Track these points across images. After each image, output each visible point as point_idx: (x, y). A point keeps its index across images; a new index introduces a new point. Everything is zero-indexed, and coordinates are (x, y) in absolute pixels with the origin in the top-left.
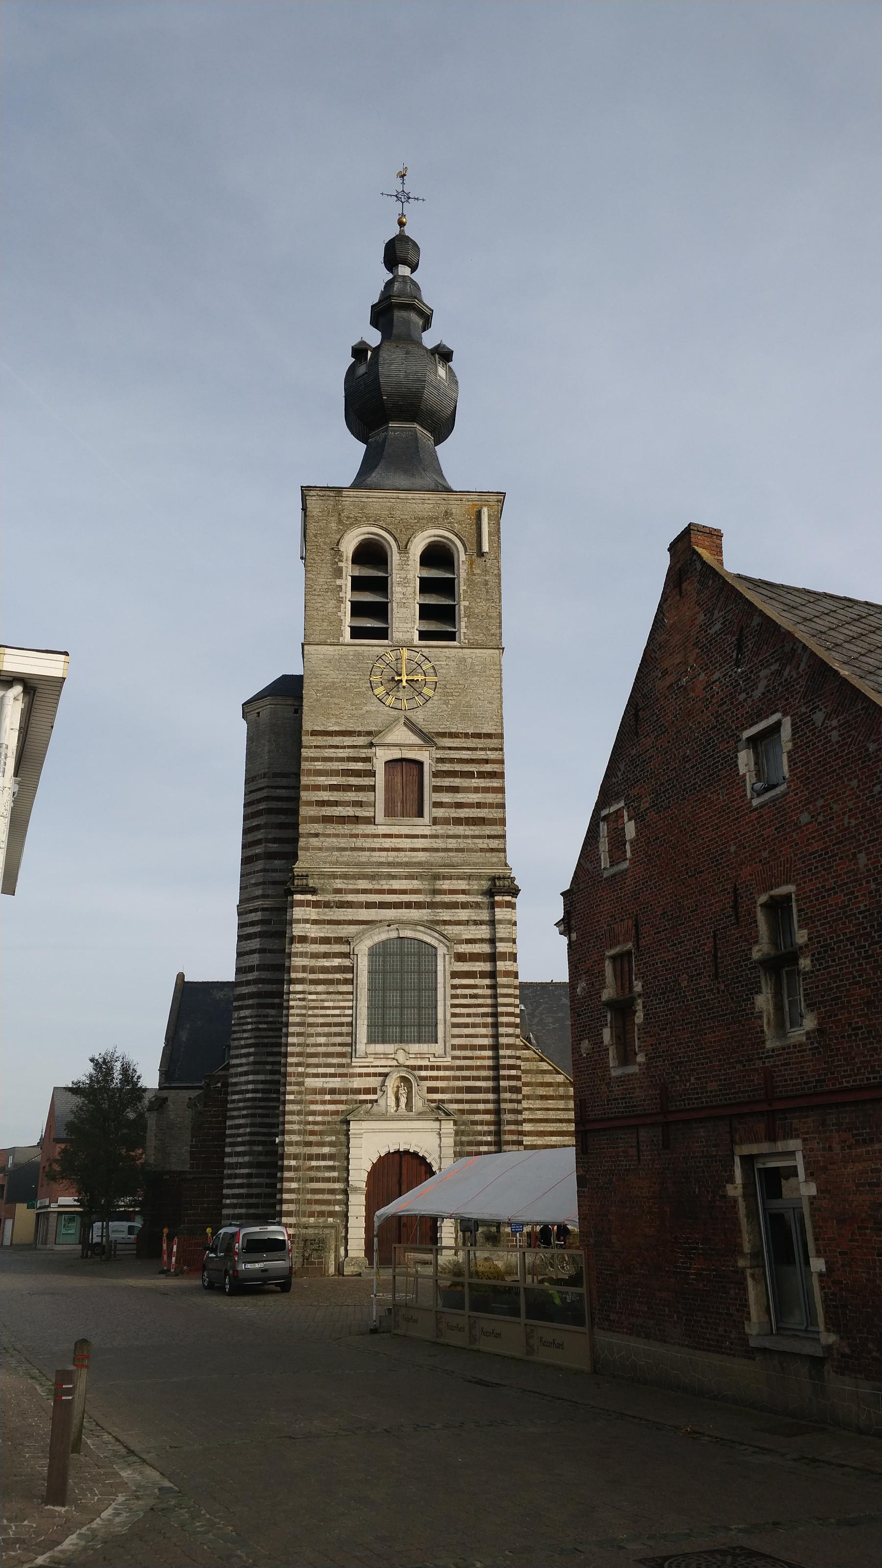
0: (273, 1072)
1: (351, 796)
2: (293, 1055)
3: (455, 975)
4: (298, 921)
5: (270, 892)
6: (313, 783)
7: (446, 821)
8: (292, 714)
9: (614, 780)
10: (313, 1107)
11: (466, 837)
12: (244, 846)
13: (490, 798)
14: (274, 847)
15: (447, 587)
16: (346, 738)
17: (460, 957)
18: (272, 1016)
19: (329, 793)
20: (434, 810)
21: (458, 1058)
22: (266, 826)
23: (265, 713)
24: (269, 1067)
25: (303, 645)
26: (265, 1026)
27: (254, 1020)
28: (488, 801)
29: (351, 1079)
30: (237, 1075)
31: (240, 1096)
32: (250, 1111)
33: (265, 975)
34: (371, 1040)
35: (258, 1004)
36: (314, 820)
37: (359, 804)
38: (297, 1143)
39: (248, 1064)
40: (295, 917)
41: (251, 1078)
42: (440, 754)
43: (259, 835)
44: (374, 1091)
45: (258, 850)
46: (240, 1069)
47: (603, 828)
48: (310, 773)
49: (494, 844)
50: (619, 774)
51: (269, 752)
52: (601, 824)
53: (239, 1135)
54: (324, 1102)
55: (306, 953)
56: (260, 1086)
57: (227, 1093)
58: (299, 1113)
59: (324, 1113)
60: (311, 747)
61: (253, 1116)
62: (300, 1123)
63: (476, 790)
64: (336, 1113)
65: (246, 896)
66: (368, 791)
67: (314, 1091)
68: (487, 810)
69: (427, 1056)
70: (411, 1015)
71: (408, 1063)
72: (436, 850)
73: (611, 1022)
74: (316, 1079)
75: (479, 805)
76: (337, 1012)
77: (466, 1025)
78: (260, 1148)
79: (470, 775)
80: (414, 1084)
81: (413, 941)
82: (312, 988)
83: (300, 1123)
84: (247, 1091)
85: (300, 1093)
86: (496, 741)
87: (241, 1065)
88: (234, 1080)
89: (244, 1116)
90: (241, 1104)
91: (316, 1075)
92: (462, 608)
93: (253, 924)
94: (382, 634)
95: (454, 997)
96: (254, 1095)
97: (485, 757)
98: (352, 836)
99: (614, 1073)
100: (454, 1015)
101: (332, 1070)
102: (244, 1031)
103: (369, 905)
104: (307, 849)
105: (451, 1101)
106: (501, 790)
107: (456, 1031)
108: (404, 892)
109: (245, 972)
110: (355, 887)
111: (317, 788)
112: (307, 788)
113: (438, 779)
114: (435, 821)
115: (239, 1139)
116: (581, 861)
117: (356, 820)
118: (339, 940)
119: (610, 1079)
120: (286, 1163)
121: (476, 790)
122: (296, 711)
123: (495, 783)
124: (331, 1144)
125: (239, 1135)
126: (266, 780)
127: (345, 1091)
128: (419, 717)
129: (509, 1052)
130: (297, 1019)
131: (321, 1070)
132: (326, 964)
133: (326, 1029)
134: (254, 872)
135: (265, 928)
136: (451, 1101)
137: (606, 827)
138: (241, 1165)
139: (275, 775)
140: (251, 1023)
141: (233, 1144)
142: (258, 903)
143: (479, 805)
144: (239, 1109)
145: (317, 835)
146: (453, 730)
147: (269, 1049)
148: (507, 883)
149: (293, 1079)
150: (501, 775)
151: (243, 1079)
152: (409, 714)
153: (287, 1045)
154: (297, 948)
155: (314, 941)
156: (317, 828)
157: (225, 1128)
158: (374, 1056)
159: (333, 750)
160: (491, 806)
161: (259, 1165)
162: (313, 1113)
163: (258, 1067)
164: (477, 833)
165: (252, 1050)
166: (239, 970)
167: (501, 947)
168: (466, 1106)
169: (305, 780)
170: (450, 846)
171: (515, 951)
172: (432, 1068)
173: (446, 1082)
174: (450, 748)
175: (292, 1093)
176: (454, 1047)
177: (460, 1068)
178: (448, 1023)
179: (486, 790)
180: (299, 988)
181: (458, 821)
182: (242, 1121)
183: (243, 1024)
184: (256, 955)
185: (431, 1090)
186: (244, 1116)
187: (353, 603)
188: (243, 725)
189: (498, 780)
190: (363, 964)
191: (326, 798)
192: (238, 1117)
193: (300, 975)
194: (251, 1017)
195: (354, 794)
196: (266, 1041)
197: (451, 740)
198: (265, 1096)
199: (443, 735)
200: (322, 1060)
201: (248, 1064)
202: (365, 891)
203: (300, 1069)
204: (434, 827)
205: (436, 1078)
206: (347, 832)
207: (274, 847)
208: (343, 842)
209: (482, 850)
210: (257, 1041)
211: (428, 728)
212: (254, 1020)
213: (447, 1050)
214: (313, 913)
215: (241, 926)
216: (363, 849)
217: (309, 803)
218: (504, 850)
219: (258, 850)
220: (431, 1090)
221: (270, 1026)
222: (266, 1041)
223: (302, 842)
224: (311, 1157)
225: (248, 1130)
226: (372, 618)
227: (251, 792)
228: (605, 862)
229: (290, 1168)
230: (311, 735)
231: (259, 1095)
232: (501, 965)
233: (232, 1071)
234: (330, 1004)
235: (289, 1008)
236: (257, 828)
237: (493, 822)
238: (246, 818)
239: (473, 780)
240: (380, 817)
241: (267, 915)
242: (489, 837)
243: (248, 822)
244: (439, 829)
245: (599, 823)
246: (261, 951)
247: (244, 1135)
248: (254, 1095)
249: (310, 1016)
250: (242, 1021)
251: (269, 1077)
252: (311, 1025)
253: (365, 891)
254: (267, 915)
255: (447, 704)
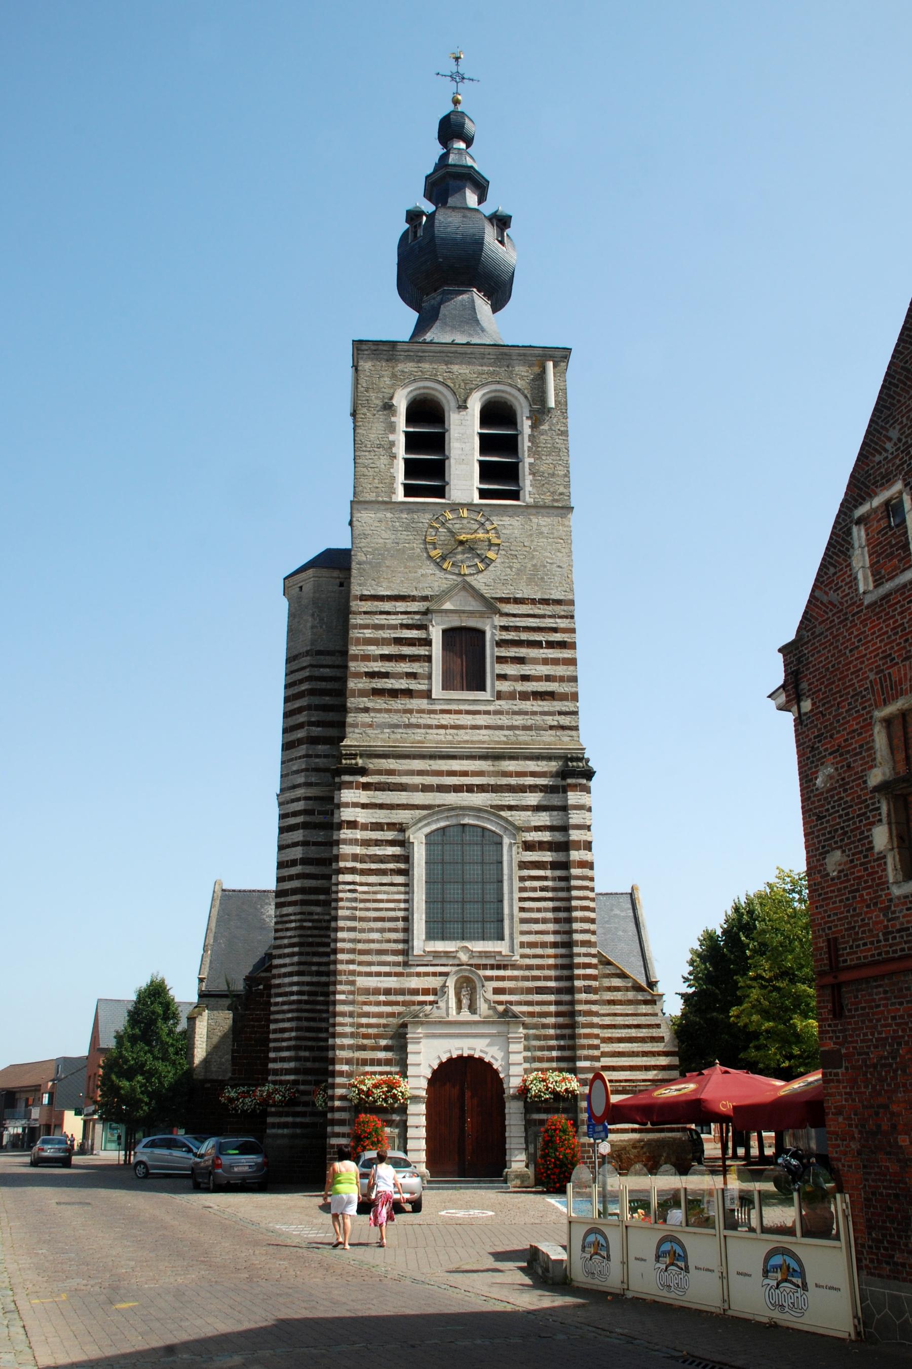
0: (319, 973)
1: (405, 667)
2: (343, 951)
3: (523, 865)
4: (347, 805)
5: (313, 780)
6: (362, 653)
7: (511, 696)
8: (337, 587)
9: (878, 458)
10: (366, 1009)
11: (534, 713)
12: (285, 731)
13: (560, 670)
14: (316, 731)
15: (510, 445)
16: (398, 604)
17: (528, 846)
18: (317, 914)
19: (380, 664)
20: (497, 683)
21: (528, 956)
22: (309, 708)
23: (308, 587)
24: (314, 968)
25: (351, 502)
26: (310, 924)
27: (298, 917)
28: (558, 674)
29: (408, 979)
30: (279, 976)
31: (285, 999)
32: (295, 1015)
33: (309, 869)
35: (301, 900)
36: (363, 693)
37: (413, 676)
38: (350, 1047)
39: (292, 964)
40: (344, 800)
41: (295, 979)
42: (504, 621)
43: (302, 718)
44: (435, 992)
45: (300, 734)
46: (283, 970)
47: (859, 535)
48: (358, 642)
49: (565, 721)
50: (888, 446)
51: (313, 627)
52: (855, 529)
53: (284, 1040)
54: (378, 1004)
55: (357, 840)
56: (306, 988)
57: (270, 996)
58: (351, 1015)
59: (379, 1015)
60: (360, 613)
61: (298, 1019)
62: (352, 1025)
63: (546, 661)
64: (392, 1015)
65: (285, 785)
66: (424, 661)
67: (367, 991)
68: (556, 684)
70: (473, 910)
71: (471, 962)
72: (501, 728)
73: (889, 815)
74: (369, 978)
75: (548, 678)
76: (392, 905)
77: (536, 921)
78: (307, 1054)
79: (537, 644)
80: (478, 985)
81: (475, 829)
82: (364, 879)
83: (352, 1025)
84: (292, 993)
85: (352, 993)
86: (565, 608)
87: (284, 965)
88: (277, 981)
89: (289, 1020)
90: (285, 1007)
91: (369, 974)
92: (527, 465)
93: (295, 814)
94: (440, 492)
95: (522, 890)
96: (300, 997)
97: (554, 625)
98: (406, 711)
99: (896, 891)
100: (522, 909)
101: (386, 969)
102: (287, 929)
103: (426, 788)
104: (355, 725)
105: (520, 1003)
106: (572, 662)
107: (526, 927)
108: (465, 774)
109: (287, 866)
110: (410, 768)
111: (366, 658)
112: (355, 658)
113: (502, 649)
114: (499, 696)
115: (284, 1044)
116: (817, 594)
117: (409, 693)
118: (391, 826)
119: (891, 900)
120: (338, 1067)
121: (546, 661)
122: (341, 585)
123: (566, 654)
124: (386, 1048)
125: (284, 1040)
126: (308, 658)
127: (401, 992)
128: (480, 582)
129: (583, 950)
130: (348, 913)
131: (375, 969)
132: (379, 853)
133: (379, 925)
134: (296, 758)
135: (308, 819)
136: (520, 1003)
137: (863, 533)
138: (288, 1072)
139: (319, 653)
140: (295, 921)
141: (277, 1049)
142: (300, 792)
143: (548, 678)
144: (283, 1012)
145: (366, 710)
146: (518, 596)
147: (314, 949)
148: (581, 764)
149: (344, 978)
150: (572, 646)
151: (287, 980)
152: (468, 579)
154: (346, 834)
155: (365, 827)
156: (364, 702)
157: (269, 1033)
159: (384, 616)
160: (562, 679)
161: (306, 1072)
162: (367, 1015)
163: (302, 968)
164: (546, 709)
165: (296, 949)
166: (280, 880)
167: (575, 835)
168: (537, 1009)
169: (353, 650)
170: (515, 723)
171: (589, 839)
173: (514, 982)
174: (514, 615)
175: (343, 993)
176: (522, 945)
177: (529, 967)
178: (516, 920)
179: (555, 662)
180: (348, 878)
181: (524, 696)
182: (287, 1025)
183: (286, 922)
184: (299, 848)
185: (497, 991)
186: (289, 1020)
187: (407, 461)
188: (285, 603)
189: (568, 651)
190: (419, 855)
191: (376, 669)
192: (283, 1020)
193: (350, 864)
194: (295, 914)
195: (408, 664)
196: (311, 940)
197: (516, 606)
198: (312, 998)
199: (506, 600)
200: (375, 958)
201: (292, 964)
202: (421, 773)
203: (352, 967)
204: (498, 702)
205: (502, 978)
206: (400, 707)
207: (316, 731)
208: (395, 719)
209: (551, 728)
210: (302, 940)
211: (488, 593)
212: (298, 917)
213: (516, 947)
214: (363, 796)
215: (282, 817)
216: (418, 726)
217: (358, 675)
218: (576, 728)
219: (300, 734)
220: (497, 991)
221: (315, 924)
222: (311, 940)
223: (350, 718)
224: (364, 1062)
225: (293, 1034)
226: (427, 470)
227: (292, 672)
228: (864, 582)
229: (341, 1074)
230: (361, 600)
231: (305, 998)
232: (575, 855)
233: (275, 971)
234: (384, 897)
235: (338, 900)
236: (299, 710)
237: (563, 697)
238: (287, 700)
239: (542, 651)
240: (437, 691)
241: (310, 805)
242: (560, 713)
243: (289, 704)
244: (504, 704)
245: (850, 529)
246: (305, 843)
247: (290, 1039)
248: (300, 997)
249: (361, 909)
250: (285, 919)
251: (315, 979)
252: (362, 919)
253: (421, 773)
254: (310, 805)
255: (511, 568)
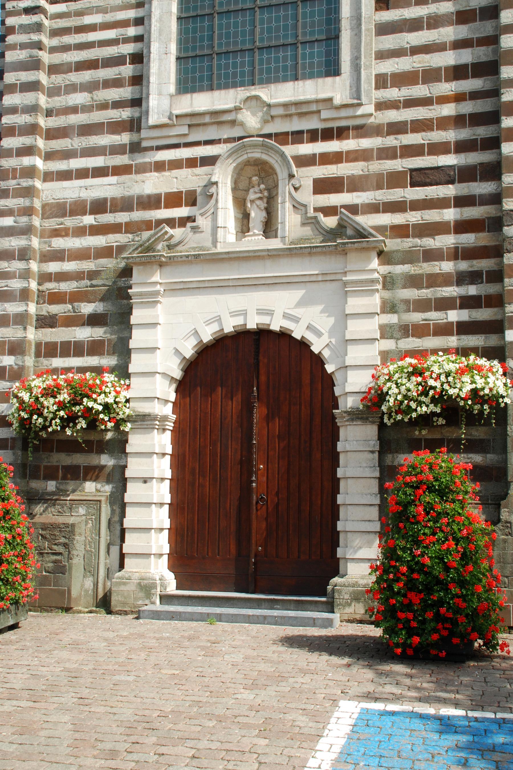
21: (394, 105)
29: (139, 177)
34: (187, 84)
54: (80, 231)
64: (106, 252)
69: (314, 107)
80: (282, 174)
89: (443, 123)
101: (98, 162)
105: (374, 208)
127: (125, 204)
130: (22, 55)
133: (87, 76)
136: (374, 208)
153: (386, 332)
158: (188, 121)
168: (413, 217)
172: (328, 134)
185: (322, 186)
205: (336, 158)
213: (364, 86)
220: (322, 186)
